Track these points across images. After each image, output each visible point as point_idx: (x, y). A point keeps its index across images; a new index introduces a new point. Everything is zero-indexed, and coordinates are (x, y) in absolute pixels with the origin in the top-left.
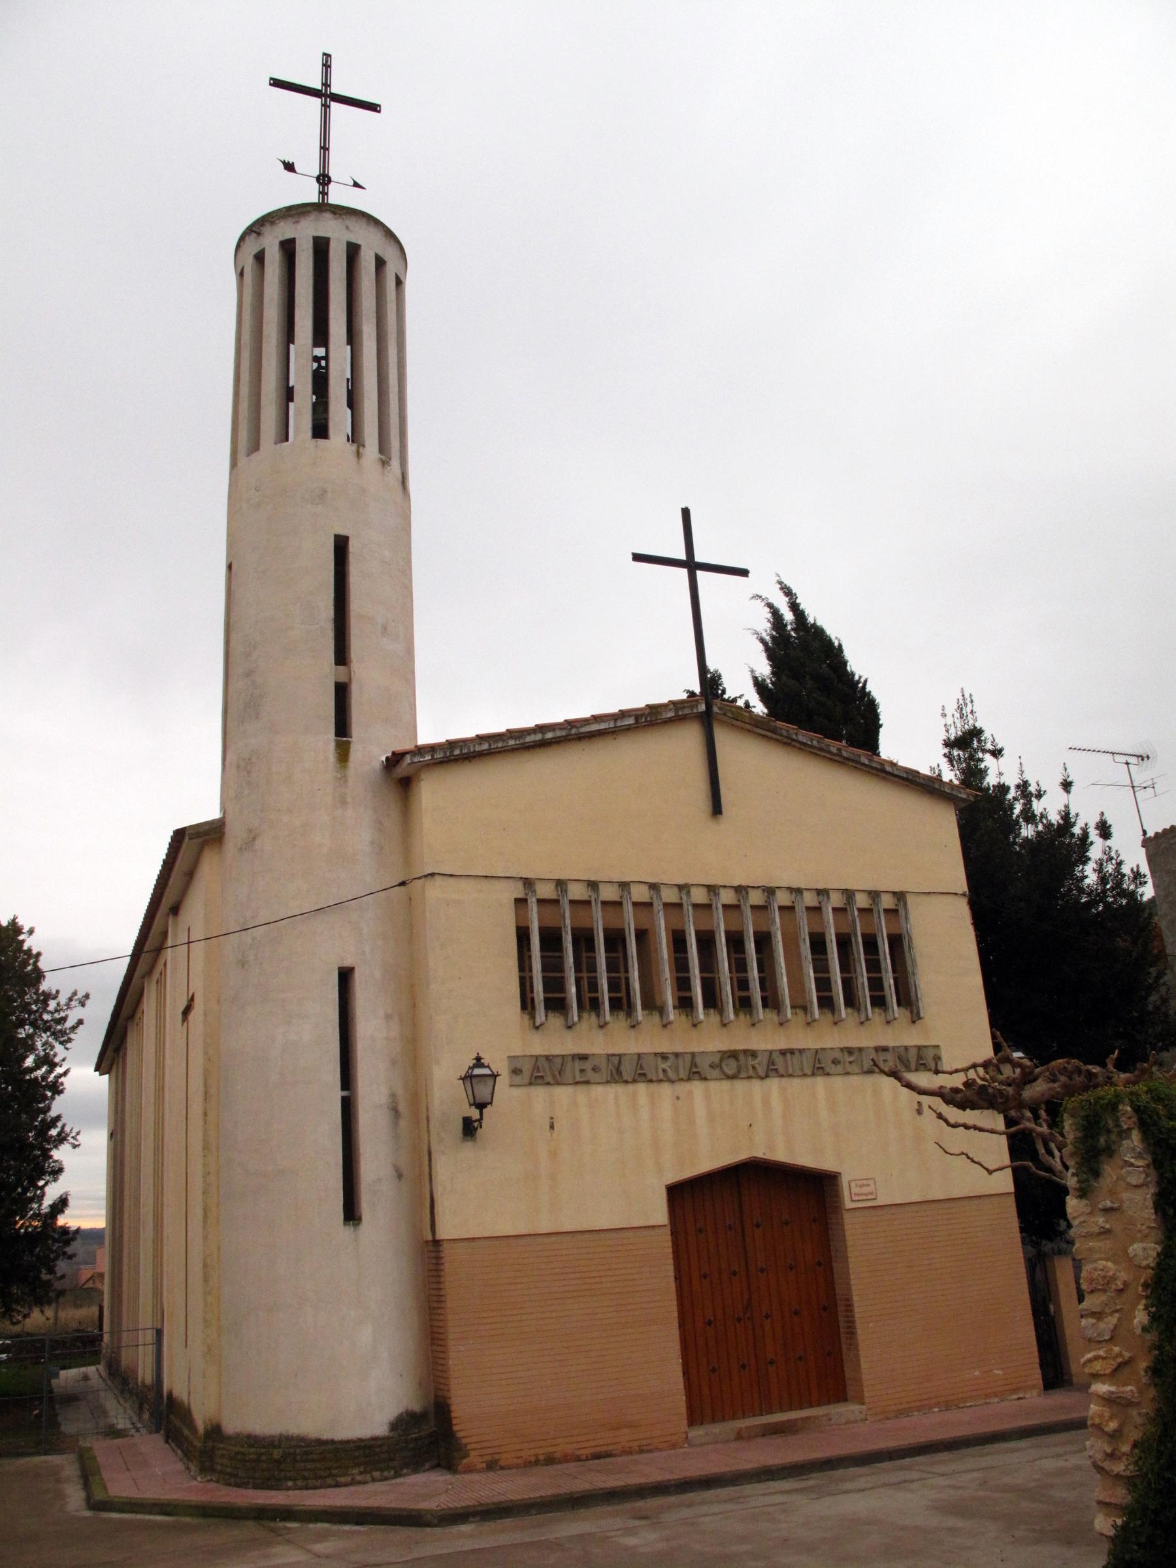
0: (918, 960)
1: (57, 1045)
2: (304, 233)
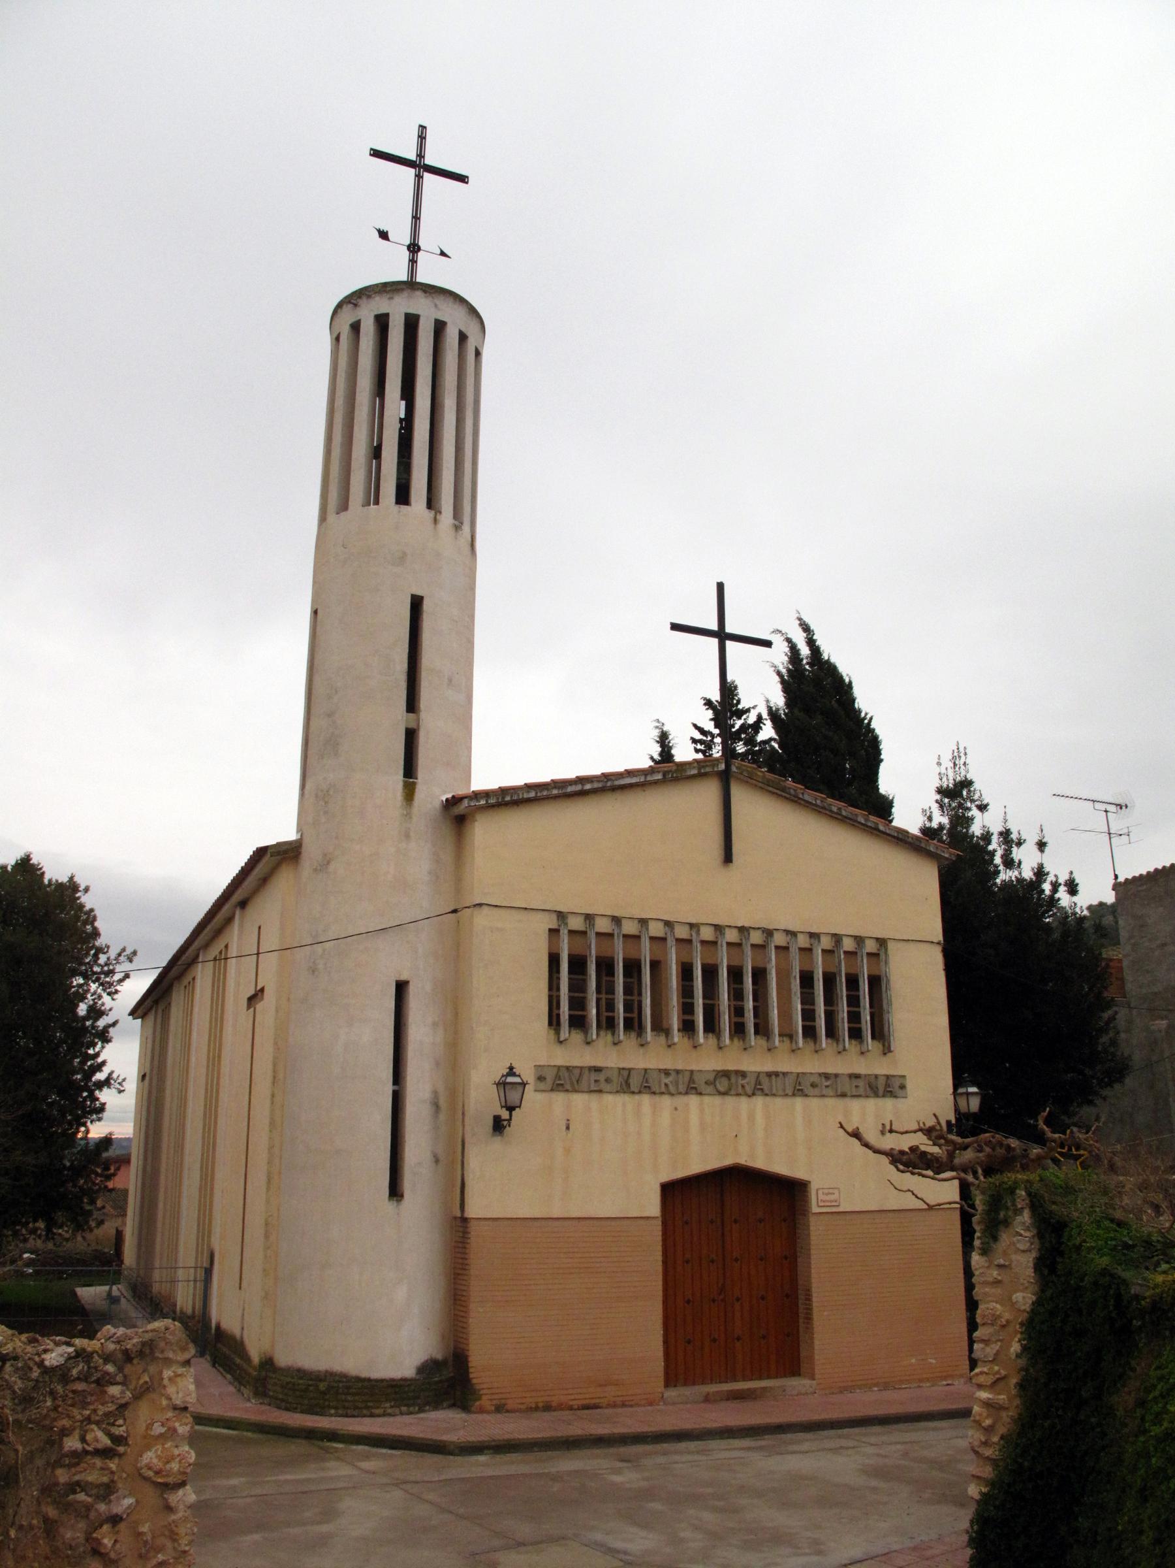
0: (893, 999)
1: (104, 995)
2: (397, 309)
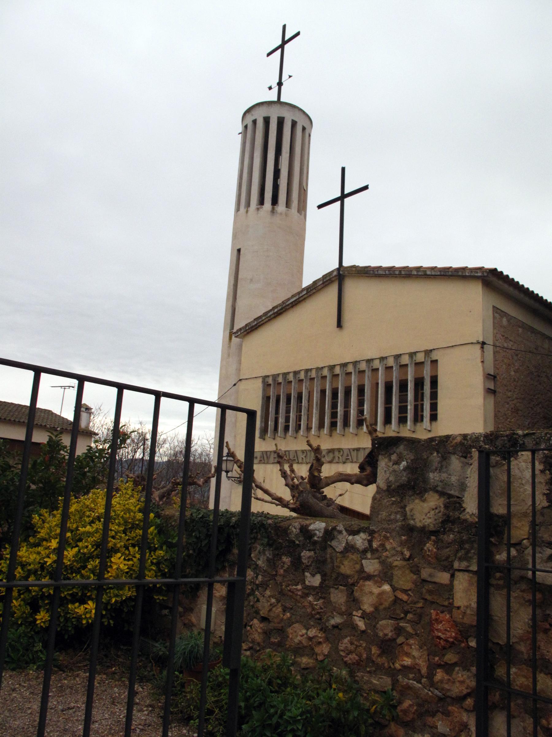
2: (274, 114)
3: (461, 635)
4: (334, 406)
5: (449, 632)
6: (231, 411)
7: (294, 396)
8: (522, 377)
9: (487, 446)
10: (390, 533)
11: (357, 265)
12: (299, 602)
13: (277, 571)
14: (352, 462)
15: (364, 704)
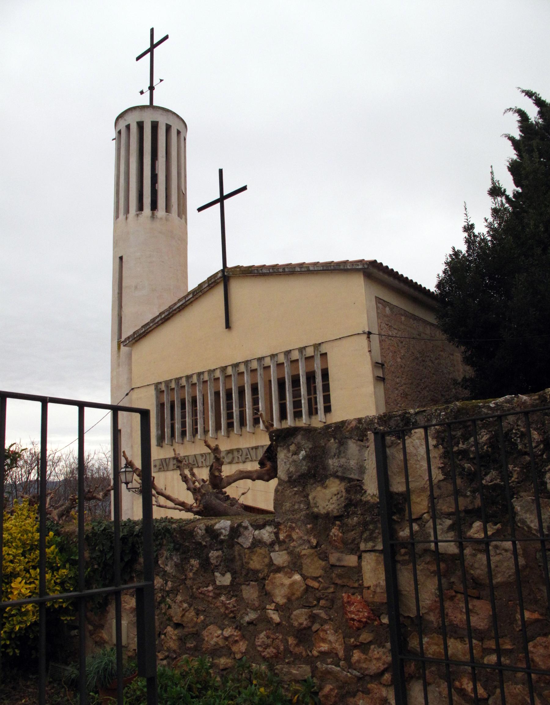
2: (148, 119)
3: (373, 614)
4: (229, 407)
5: (361, 612)
6: (125, 413)
7: (188, 401)
8: (408, 363)
9: (381, 428)
10: (296, 523)
11: (241, 265)
12: (211, 604)
13: (186, 575)
14: (252, 461)
15: (286, 696)
